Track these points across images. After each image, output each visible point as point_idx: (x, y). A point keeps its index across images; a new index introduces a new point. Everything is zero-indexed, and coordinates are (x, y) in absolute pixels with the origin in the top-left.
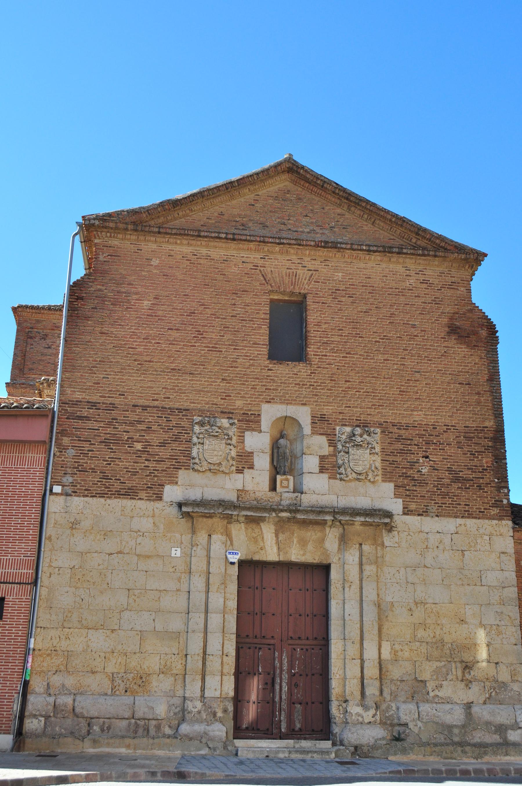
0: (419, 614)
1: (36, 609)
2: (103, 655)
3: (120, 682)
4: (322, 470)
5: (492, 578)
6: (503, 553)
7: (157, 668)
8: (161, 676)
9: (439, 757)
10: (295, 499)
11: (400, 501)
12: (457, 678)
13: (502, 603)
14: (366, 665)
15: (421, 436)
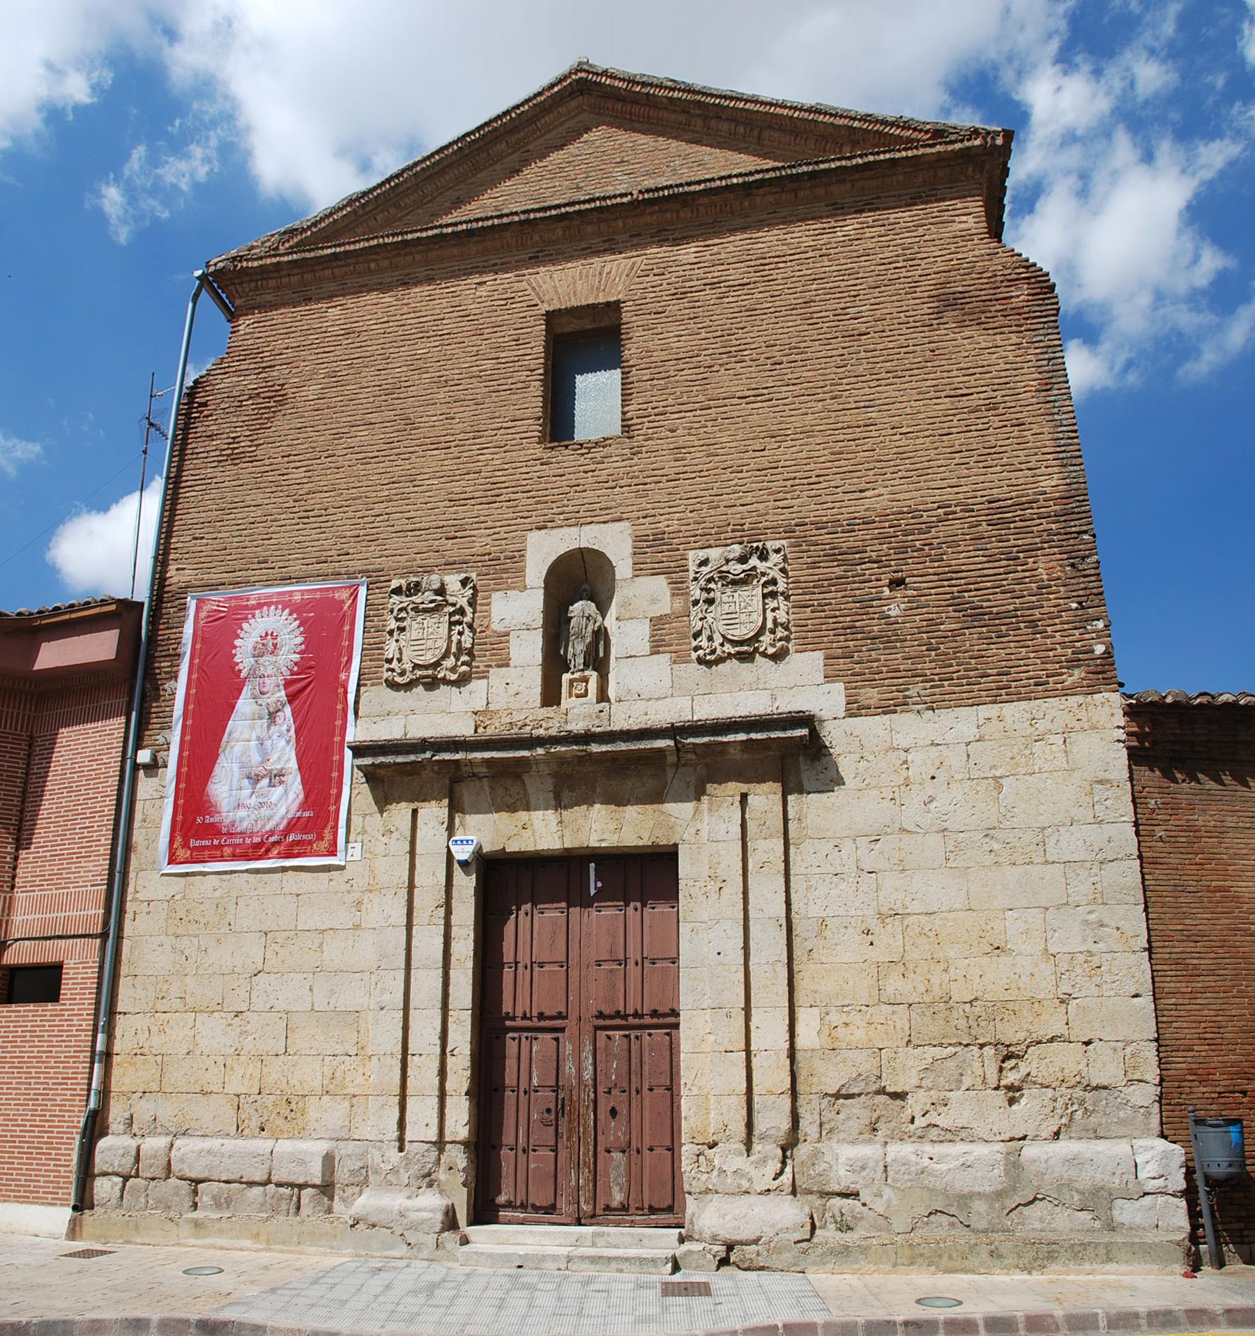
0: (889, 942)
2: (221, 1060)
3: (252, 1111)
4: (657, 647)
5: (1069, 844)
6: (1100, 782)
7: (317, 1084)
8: (326, 1098)
9: (933, 1268)
10: (598, 717)
11: (839, 687)
14: (755, 1061)
15: (883, 538)
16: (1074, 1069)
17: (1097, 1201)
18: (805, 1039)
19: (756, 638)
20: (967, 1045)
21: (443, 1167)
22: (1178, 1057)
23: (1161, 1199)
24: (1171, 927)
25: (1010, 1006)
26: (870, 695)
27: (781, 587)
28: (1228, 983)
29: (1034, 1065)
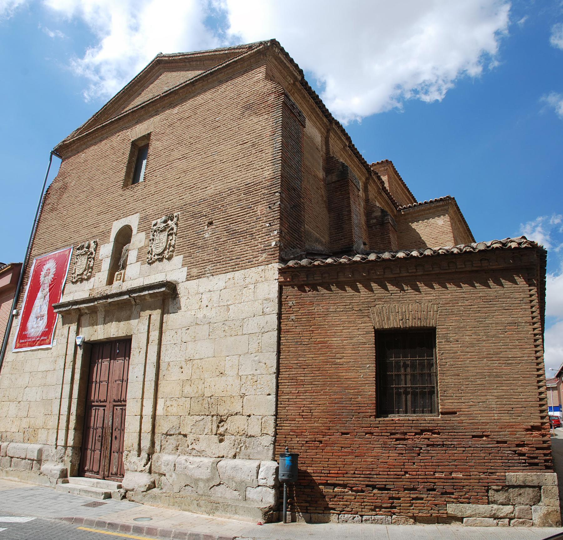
1: (64, 419)
5: (252, 326)
6: (266, 300)
12: (211, 431)
13: (260, 351)
16: (242, 427)
17: (242, 487)
18: (159, 411)
19: (163, 252)
20: (208, 415)
21: (66, 455)
22: (286, 423)
23: (265, 489)
24: (291, 362)
25: (223, 399)
26: (195, 271)
27: (175, 230)
28: (318, 388)
29: (229, 425)
